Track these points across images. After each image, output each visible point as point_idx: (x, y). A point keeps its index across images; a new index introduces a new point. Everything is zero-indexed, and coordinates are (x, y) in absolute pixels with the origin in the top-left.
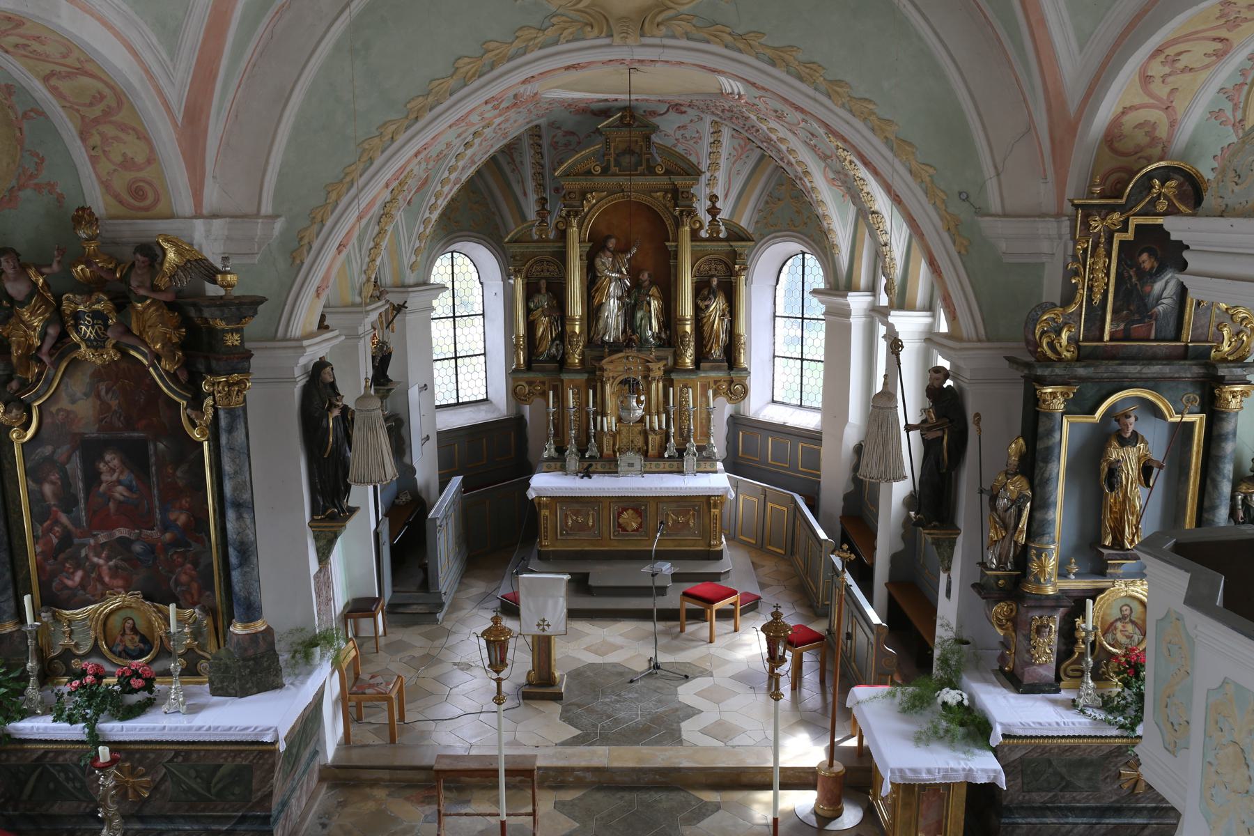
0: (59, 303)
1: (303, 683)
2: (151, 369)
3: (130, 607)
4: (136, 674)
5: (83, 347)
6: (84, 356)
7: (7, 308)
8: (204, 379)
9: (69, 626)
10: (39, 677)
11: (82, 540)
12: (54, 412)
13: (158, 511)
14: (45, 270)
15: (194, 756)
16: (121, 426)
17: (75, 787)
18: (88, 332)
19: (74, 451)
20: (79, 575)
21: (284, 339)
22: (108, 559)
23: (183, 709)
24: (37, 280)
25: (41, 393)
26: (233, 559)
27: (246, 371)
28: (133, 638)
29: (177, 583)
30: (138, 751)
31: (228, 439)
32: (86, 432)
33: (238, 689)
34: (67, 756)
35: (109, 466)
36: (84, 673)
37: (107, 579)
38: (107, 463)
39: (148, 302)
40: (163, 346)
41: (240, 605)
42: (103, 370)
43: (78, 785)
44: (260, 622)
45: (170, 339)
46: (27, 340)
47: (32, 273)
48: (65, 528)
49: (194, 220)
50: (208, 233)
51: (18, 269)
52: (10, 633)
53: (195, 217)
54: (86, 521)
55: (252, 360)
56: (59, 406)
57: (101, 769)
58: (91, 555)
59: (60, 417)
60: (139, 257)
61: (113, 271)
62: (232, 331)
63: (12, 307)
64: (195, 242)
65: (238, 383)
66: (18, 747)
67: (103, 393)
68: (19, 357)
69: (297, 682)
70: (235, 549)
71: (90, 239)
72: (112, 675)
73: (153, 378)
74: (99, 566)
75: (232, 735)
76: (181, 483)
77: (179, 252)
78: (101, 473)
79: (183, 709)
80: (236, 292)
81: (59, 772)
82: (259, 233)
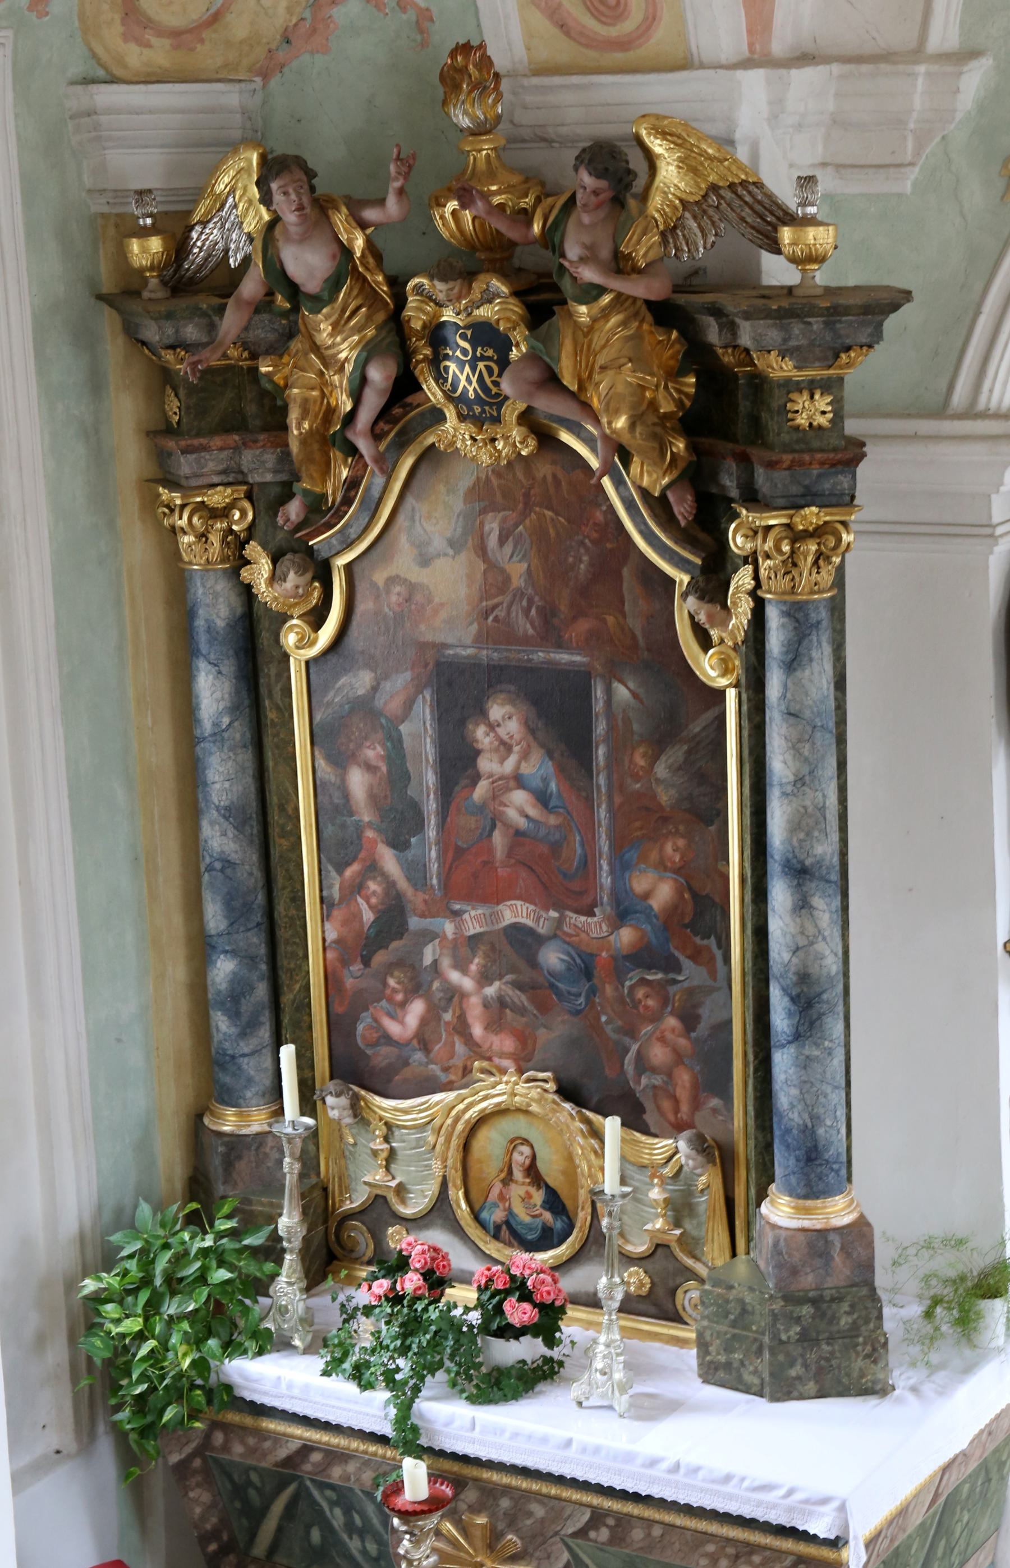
0: (400, 301)
1: (943, 1392)
2: (606, 482)
3: (526, 1112)
4: (523, 1292)
5: (450, 413)
6: (452, 443)
7: (285, 314)
8: (736, 515)
9: (386, 1139)
10: (306, 1254)
11: (427, 923)
12: (381, 584)
13: (605, 867)
14: (370, 214)
15: (637, 1534)
16: (531, 631)
17: (364, 1552)
18: (463, 378)
19: (419, 691)
20: (417, 1008)
21: (971, 413)
22: (485, 978)
23: (622, 1402)
24: (350, 240)
25: (353, 533)
26: (780, 1020)
27: (847, 500)
28: (529, 1196)
29: (642, 1065)
30: (507, 1490)
31: (785, 686)
32: (450, 640)
33: (766, 1375)
34: (351, 1467)
35: (498, 737)
36: (402, 1264)
37: (477, 1031)
38: (492, 727)
39: (606, 299)
40: (632, 425)
41: (788, 1146)
42: (495, 481)
43: (372, 1548)
44: (839, 1202)
45: (653, 405)
46: (323, 395)
47: (340, 220)
48: (390, 885)
49: (740, 74)
50: (777, 105)
51: (308, 210)
52: (258, 1134)
53: (747, 64)
54: (439, 874)
55: (863, 470)
56: (391, 570)
57: (405, 1515)
58: (446, 963)
59: (394, 598)
60: (586, 178)
61: (525, 216)
62: (812, 387)
63: (296, 309)
64: (738, 136)
65: (818, 532)
66: (248, 1421)
67: (493, 541)
68: (304, 441)
69: (927, 1388)
70: (785, 990)
71: (480, 130)
72: (465, 1279)
73: (611, 509)
74: (463, 995)
75: (731, 1497)
76: (665, 797)
77: (690, 165)
78: (478, 752)
79: (622, 1402)
80: (822, 277)
81: (333, 1504)
82: (918, 102)
